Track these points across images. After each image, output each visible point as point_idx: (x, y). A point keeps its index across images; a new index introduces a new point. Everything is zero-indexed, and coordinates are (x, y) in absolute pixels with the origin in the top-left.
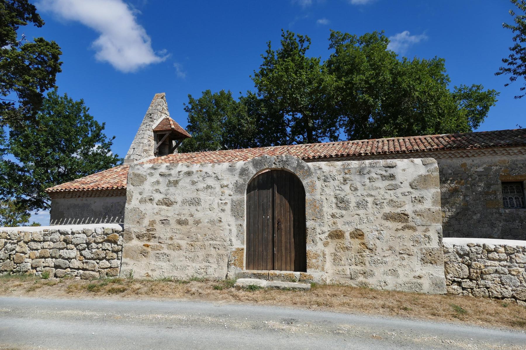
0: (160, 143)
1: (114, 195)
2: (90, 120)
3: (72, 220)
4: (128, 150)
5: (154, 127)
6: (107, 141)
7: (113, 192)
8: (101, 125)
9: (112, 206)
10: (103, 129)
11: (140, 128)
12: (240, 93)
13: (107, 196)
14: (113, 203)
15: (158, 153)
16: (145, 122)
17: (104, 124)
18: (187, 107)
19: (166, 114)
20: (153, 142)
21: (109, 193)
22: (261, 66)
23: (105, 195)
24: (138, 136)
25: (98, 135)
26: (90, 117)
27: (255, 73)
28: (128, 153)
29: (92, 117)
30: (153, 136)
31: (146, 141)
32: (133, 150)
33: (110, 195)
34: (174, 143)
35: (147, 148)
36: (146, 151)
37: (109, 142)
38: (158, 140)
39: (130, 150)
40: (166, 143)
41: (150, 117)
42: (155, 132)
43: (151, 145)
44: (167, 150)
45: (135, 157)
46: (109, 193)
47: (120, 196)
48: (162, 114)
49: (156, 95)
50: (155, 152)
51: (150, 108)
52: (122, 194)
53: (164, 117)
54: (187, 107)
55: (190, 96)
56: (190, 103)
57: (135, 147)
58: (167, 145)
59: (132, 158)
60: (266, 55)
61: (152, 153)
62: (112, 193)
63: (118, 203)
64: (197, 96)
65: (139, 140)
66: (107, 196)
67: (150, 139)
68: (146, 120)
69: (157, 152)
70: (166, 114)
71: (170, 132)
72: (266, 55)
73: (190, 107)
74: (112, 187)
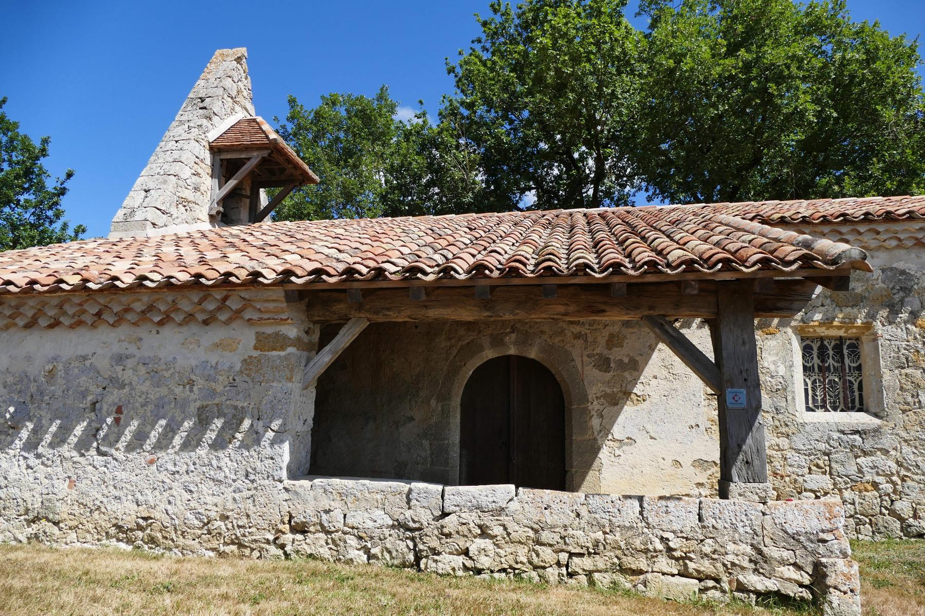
0: (232, 183)
1: (66, 321)
2: (8, 130)
3: (171, 430)
4: (126, 194)
5: (213, 135)
6: (50, 185)
7: (60, 306)
8: (37, 144)
9: (51, 374)
10: (44, 156)
11: (167, 133)
12: (421, 102)
13: (27, 326)
14: (55, 359)
15: (219, 218)
16: (184, 118)
17: (45, 141)
18: (283, 127)
19: (247, 111)
20: (208, 183)
21: (39, 313)
22: (473, 42)
23: (21, 322)
24: (161, 155)
25: (28, 172)
26: (8, 122)
27: (446, 64)
28: (128, 202)
29: (16, 125)
30: (208, 161)
31: (186, 173)
32: (144, 193)
33: (43, 322)
34: (264, 198)
35: (188, 194)
36: (183, 202)
37: (55, 188)
38: (223, 179)
39: (131, 193)
40: (244, 192)
41: (201, 105)
42: (215, 150)
43: (203, 188)
44: (244, 214)
45: (152, 215)
46: (39, 313)
47: (94, 326)
48: (237, 108)
49: (218, 52)
50: (214, 212)
51: (201, 83)
52: (105, 316)
53: (240, 115)
54: (283, 127)
55: (292, 102)
56: (292, 119)
57: (151, 185)
58: (247, 197)
59: (139, 216)
60: (488, 15)
61: (203, 213)
62: (52, 312)
63: (85, 358)
64: (310, 104)
65: (166, 166)
66: (31, 325)
67: (200, 171)
68: (188, 114)
69: (218, 212)
70: (247, 111)
71: (265, 153)
72: (488, 15)
73: (290, 127)
74: (53, 279)
